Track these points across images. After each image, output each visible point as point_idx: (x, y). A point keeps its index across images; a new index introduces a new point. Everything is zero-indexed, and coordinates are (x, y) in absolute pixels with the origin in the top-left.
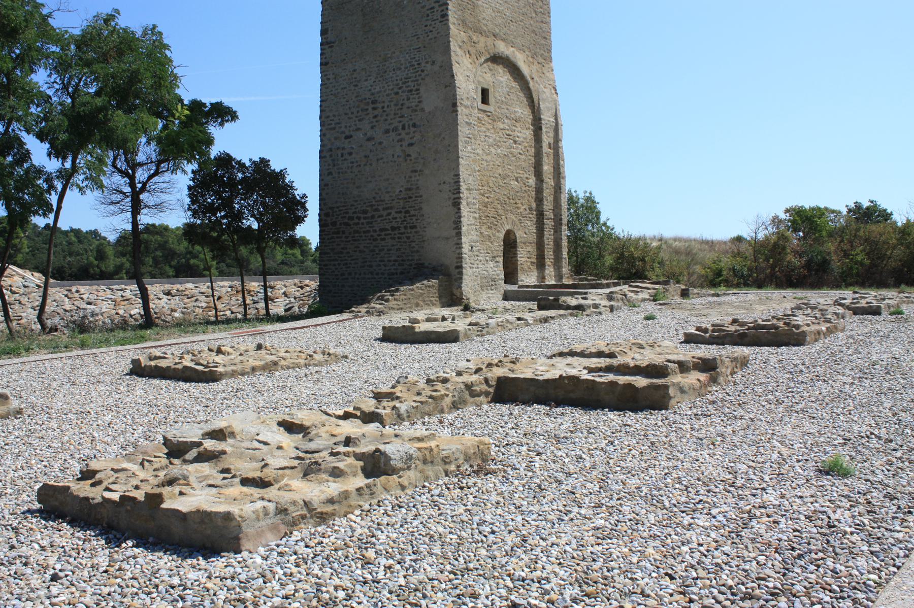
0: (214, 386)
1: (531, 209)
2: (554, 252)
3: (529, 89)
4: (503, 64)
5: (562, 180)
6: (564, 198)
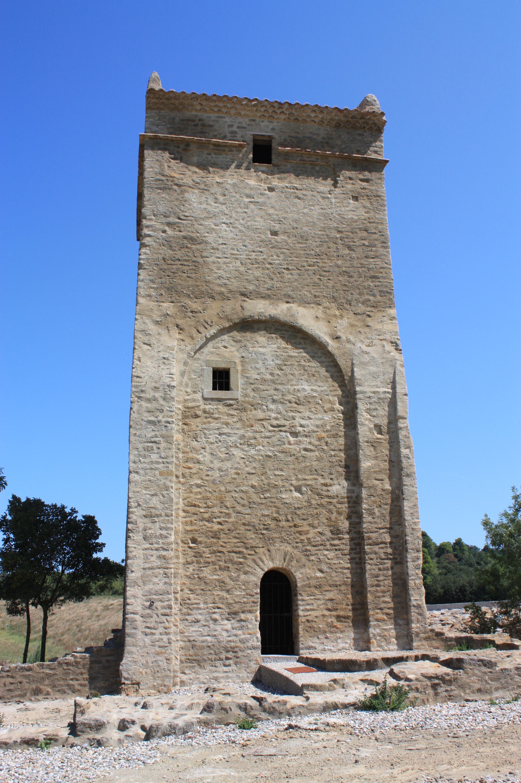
0: (254, 695)
1: (336, 532)
2: (394, 597)
3: (329, 355)
4: (265, 329)
5: (406, 481)
6: (414, 542)
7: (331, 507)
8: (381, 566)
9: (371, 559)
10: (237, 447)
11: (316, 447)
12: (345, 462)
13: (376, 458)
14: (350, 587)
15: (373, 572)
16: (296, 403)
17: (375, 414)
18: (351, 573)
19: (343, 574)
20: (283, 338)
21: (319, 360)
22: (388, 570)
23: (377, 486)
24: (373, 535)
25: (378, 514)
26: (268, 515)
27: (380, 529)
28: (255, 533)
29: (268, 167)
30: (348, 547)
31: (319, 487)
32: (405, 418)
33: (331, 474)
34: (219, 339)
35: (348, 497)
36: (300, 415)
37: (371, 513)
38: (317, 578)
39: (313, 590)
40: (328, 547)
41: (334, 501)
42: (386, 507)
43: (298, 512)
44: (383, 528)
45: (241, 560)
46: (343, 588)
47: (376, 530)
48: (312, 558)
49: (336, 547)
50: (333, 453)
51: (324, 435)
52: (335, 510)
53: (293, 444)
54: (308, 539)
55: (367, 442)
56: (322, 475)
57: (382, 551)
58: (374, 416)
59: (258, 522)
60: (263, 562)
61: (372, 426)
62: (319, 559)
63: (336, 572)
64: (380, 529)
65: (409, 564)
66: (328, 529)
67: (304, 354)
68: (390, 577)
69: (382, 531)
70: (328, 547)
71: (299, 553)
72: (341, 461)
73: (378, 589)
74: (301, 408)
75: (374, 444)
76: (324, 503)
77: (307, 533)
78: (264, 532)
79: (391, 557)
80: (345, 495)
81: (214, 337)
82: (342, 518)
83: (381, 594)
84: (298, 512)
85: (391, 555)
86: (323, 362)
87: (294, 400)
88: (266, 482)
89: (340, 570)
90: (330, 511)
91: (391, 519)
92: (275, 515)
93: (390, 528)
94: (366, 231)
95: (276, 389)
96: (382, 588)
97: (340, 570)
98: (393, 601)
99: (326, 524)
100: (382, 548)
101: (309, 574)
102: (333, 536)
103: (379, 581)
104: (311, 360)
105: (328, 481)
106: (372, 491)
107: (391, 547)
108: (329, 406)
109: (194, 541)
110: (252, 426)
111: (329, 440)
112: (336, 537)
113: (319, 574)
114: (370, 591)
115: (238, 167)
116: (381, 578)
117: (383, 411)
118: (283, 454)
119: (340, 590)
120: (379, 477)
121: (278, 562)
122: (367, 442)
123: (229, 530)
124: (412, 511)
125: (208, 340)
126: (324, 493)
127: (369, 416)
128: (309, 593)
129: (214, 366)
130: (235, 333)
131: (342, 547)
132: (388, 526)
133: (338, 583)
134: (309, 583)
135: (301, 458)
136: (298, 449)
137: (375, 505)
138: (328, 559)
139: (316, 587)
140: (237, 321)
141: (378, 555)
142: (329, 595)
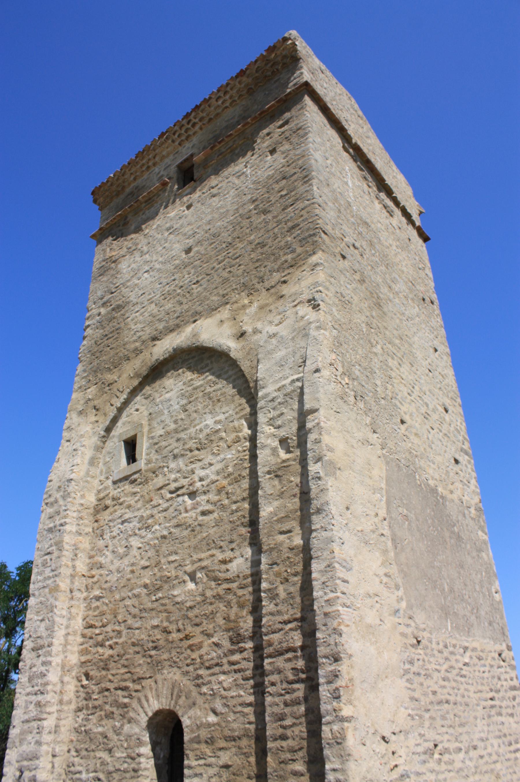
1: (237, 639)
7: (230, 597)
8: (288, 697)
9: (273, 684)
10: (136, 535)
11: (215, 504)
12: (250, 517)
13: (281, 495)
14: (253, 741)
15: (276, 709)
16: (198, 449)
17: (279, 422)
18: (255, 712)
19: (245, 715)
20: (189, 369)
21: (226, 376)
22: (299, 704)
23: (281, 544)
24: (275, 637)
25: (282, 594)
26: (158, 626)
27: (286, 623)
28: (144, 656)
29: (189, 187)
30: (251, 664)
31: (217, 568)
32: (316, 410)
33: (231, 542)
34: (132, 403)
35: (252, 575)
36: (199, 464)
37: (274, 597)
38: (209, 725)
39: (203, 747)
40: (226, 667)
41: (234, 585)
42: (296, 579)
43: (191, 614)
44: (290, 622)
45: (126, 700)
46: (244, 742)
47: (280, 626)
48: (204, 689)
49: (236, 667)
50: (234, 507)
51: (225, 482)
52: (234, 601)
53: (189, 509)
54: (201, 657)
55: (269, 473)
56: (221, 547)
57: (289, 665)
58: (279, 427)
59: (147, 638)
60: (147, 701)
61: (276, 443)
62: (212, 690)
63: (235, 713)
64: (286, 623)
65: (321, 689)
66: (226, 635)
67: (210, 377)
68: (303, 719)
69: (290, 626)
70: (226, 667)
71: (188, 682)
72: (244, 517)
73: (284, 744)
74: (201, 454)
75: (279, 473)
76: (222, 593)
77: (200, 646)
78: (153, 653)
79: (304, 676)
80: (248, 572)
81: (126, 403)
82: (244, 613)
83: (288, 756)
84: (191, 614)
85: (303, 672)
86: (230, 377)
87: (195, 446)
88: (159, 574)
89: (239, 708)
90: (229, 605)
91: (302, 601)
92: (165, 624)
93: (302, 619)
94: (284, 178)
95: (178, 440)
96: (290, 742)
97: (239, 708)
98: (309, 770)
99: (223, 627)
100: (289, 660)
101: (199, 717)
102: (233, 647)
103: (284, 727)
104: (217, 381)
105: (228, 554)
106: (275, 554)
107: (303, 656)
108: (233, 436)
109: (87, 676)
110: (152, 500)
111: (230, 489)
112: (236, 648)
113: (212, 719)
114: (270, 749)
115: (166, 207)
116: (288, 722)
117: (291, 415)
118: (179, 529)
119: (239, 748)
120: (286, 527)
121: (164, 700)
122: (269, 473)
123: (118, 656)
124: (323, 579)
125: (120, 410)
126: (222, 575)
127: (273, 430)
128: (199, 753)
129: (125, 438)
130: (147, 390)
131: (244, 665)
132: (299, 615)
133: (236, 734)
134: (199, 736)
135: (198, 528)
136: (194, 515)
137: (279, 580)
138: (225, 690)
139: (206, 742)
140: (145, 373)
141: (282, 675)
142: (225, 758)
